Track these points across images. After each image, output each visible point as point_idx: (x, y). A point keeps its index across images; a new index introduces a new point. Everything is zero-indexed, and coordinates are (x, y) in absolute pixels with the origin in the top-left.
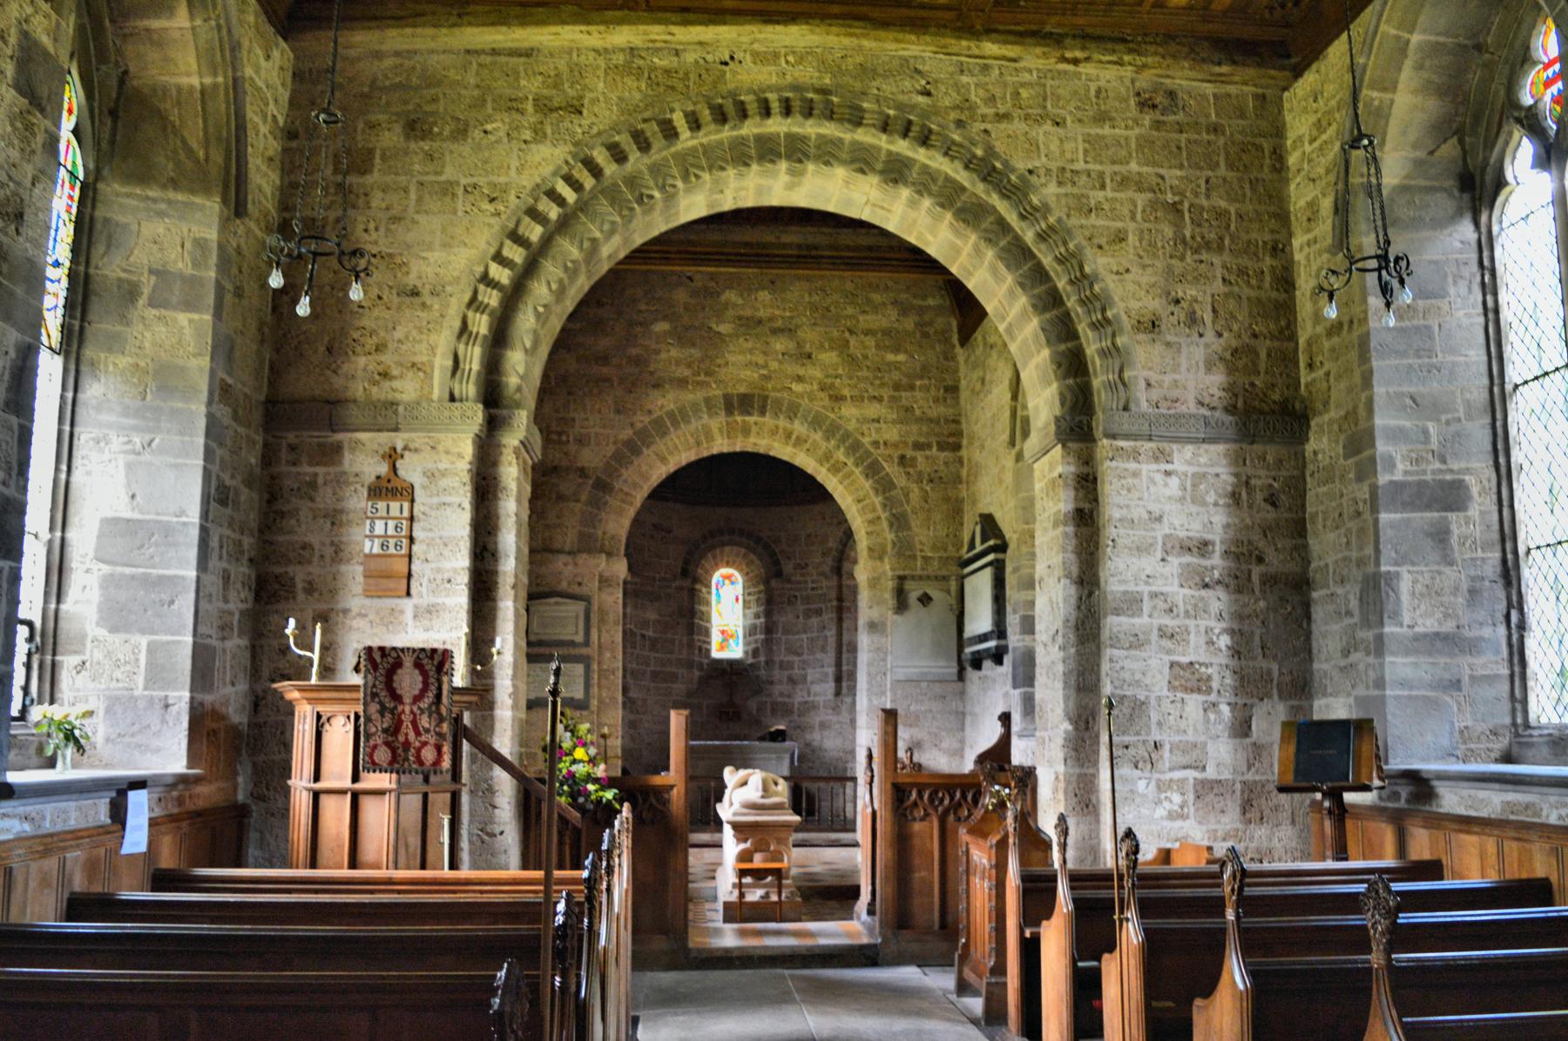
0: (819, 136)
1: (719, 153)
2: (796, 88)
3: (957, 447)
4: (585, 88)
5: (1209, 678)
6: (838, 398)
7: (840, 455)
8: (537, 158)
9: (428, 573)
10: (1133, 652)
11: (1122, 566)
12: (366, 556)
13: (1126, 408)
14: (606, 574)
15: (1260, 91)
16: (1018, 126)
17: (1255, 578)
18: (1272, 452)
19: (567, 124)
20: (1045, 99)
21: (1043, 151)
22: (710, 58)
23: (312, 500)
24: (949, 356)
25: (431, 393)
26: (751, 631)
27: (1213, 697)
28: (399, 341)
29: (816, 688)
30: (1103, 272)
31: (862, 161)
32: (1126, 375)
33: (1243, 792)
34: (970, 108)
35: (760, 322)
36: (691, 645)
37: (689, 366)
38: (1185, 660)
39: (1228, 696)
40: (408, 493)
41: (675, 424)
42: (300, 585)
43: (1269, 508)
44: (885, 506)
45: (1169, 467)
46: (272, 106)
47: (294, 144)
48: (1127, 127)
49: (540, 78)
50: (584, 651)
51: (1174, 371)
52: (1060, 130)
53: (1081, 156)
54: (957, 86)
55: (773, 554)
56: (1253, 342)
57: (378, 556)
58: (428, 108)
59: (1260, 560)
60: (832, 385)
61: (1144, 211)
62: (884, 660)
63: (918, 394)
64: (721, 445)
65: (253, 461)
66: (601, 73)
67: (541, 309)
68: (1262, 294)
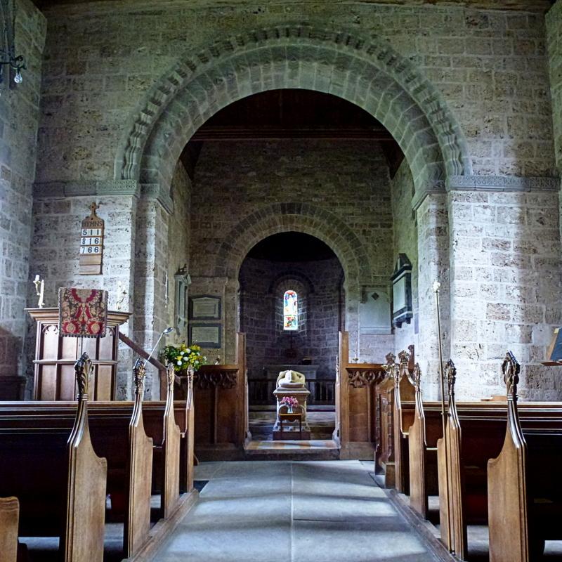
0: (304, 47)
1: (254, 58)
2: (290, 22)
3: (390, 226)
4: (187, 28)
5: (508, 312)
6: (334, 204)
7: (335, 230)
8: (164, 62)
9: (111, 263)
10: (467, 298)
11: (461, 254)
12: (81, 255)
13: (462, 174)
14: (229, 287)
15: (533, 14)
16: (405, 36)
17: (532, 261)
18: (541, 196)
19: (178, 45)
20: (418, 23)
21: (418, 49)
22: (248, 10)
23: (56, 229)
24: (385, 184)
25: (113, 176)
26: (301, 317)
27: (511, 322)
28: (98, 152)
29: (329, 342)
30: (449, 108)
31: (325, 58)
32: (463, 157)
33: (527, 371)
34: (380, 29)
35: (297, 170)
36: (274, 323)
37: (265, 191)
38: (495, 302)
39: (519, 322)
40: (101, 224)
41: (259, 217)
42: (50, 271)
43: (539, 224)
44: (356, 253)
45: (486, 204)
46: (34, 41)
47: (48, 62)
48: (461, 35)
49: (165, 24)
50: (218, 322)
51: (487, 156)
52: (426, 38)
53: (437, 50)
54: (373, 18)
55: (310, 282)
56: (529, 140)
57: (87, 255)
58: (111, 41)
59: (535, 251)
60: (331, 199)
61: (471, 76)
62: (357, 325)
63: (371, 202)
64: (281, 229)
65: (26, 211)
66: (195, 20)
67: (167, 136)
68: (534, 116)
